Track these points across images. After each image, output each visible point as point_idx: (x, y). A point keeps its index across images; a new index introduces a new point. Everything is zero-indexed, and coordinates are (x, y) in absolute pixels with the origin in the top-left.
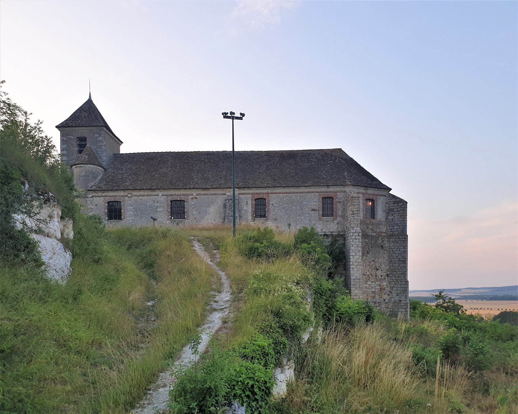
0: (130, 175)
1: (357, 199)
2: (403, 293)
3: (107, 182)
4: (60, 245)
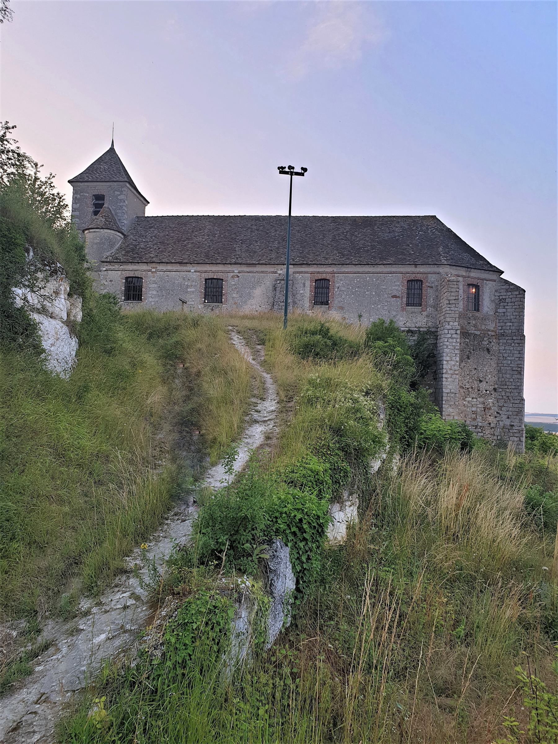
0: (156, 244)
2: (517, 415)
3: (128, 252)
4: (65, 329)
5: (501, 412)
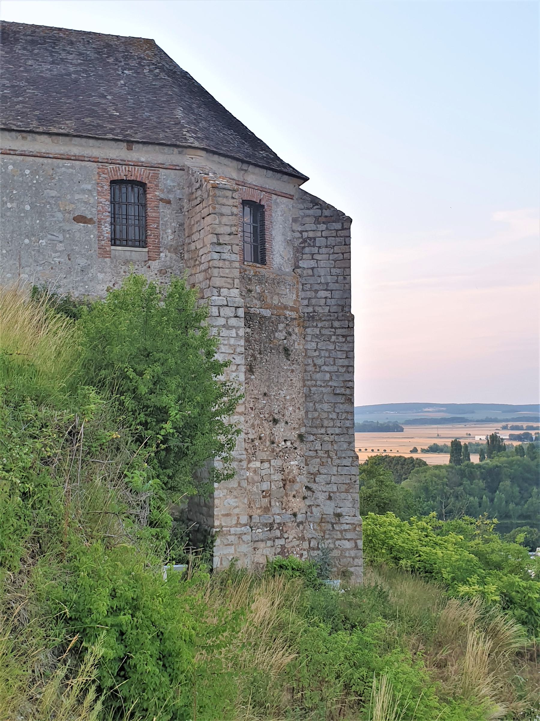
1: (229, 194)
2: (347, 491)
5: (313, 486)
